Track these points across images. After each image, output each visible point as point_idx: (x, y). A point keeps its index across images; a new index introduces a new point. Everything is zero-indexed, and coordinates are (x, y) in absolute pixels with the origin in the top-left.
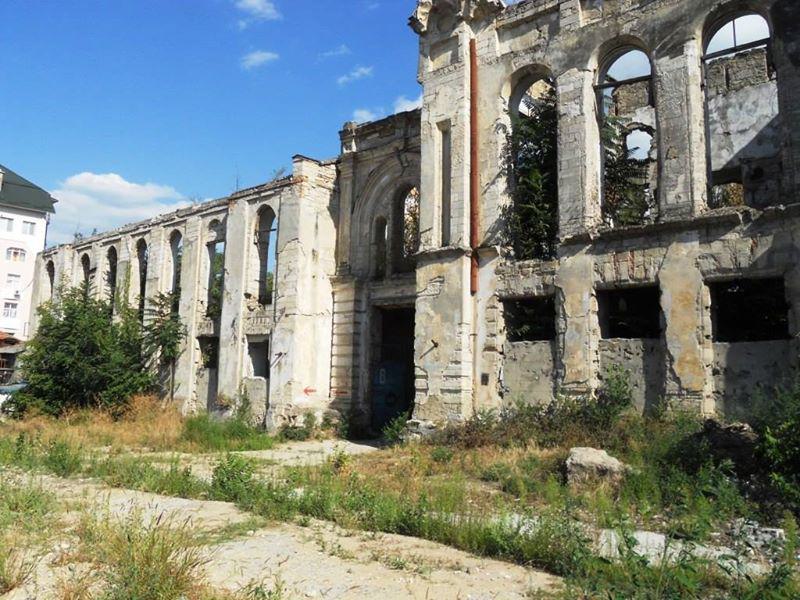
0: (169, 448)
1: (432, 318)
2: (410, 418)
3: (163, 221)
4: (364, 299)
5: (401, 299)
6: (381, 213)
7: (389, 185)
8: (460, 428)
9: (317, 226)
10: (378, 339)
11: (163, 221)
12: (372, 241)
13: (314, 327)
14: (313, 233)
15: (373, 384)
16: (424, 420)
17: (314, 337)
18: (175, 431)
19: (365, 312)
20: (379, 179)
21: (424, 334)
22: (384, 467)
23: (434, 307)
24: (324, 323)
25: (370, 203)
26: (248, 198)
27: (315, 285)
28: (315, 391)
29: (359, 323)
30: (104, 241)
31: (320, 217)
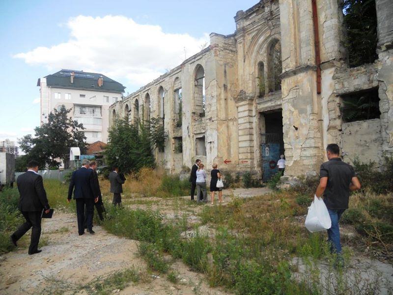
0: (154, 195)
1: (293, 112)
2: (283, 175)
3: (155, 83)
4: (254, 108)
5: (274, 106)
6: (260, 59)
7: (264, 42)
8: (269, 81)
9: (225, 72)
10: (263, 132)
11: (155, 83)
12: (257, 76)
13: (228, 127)
14: (223, 75)
15: (262, 156)
16: (291, 176)
17: (228, 132)
18: (158, 184)
19: (254, 116)
20: (258, 40)
21: (288, 123)
22: (265, 207)
23: (294, 106)
24: (233, 124)
25: (254, 54)
26: (190, 62)
27: (226, 104)
28: (230, 162)
29: (252, 123)
30: (133, 97)
31: (226, 66)
